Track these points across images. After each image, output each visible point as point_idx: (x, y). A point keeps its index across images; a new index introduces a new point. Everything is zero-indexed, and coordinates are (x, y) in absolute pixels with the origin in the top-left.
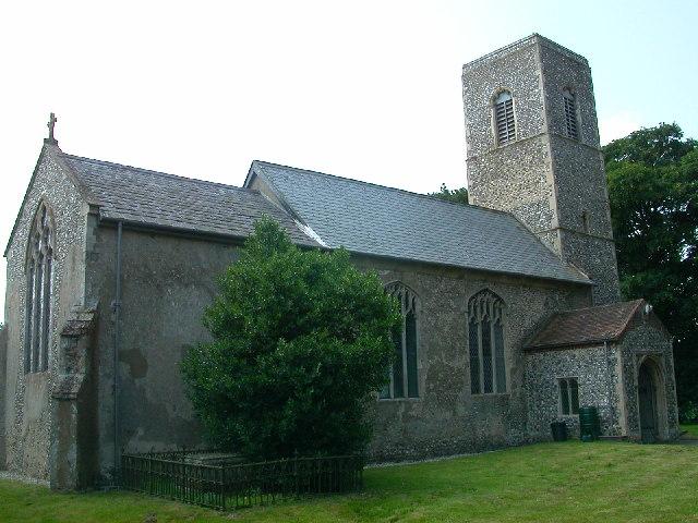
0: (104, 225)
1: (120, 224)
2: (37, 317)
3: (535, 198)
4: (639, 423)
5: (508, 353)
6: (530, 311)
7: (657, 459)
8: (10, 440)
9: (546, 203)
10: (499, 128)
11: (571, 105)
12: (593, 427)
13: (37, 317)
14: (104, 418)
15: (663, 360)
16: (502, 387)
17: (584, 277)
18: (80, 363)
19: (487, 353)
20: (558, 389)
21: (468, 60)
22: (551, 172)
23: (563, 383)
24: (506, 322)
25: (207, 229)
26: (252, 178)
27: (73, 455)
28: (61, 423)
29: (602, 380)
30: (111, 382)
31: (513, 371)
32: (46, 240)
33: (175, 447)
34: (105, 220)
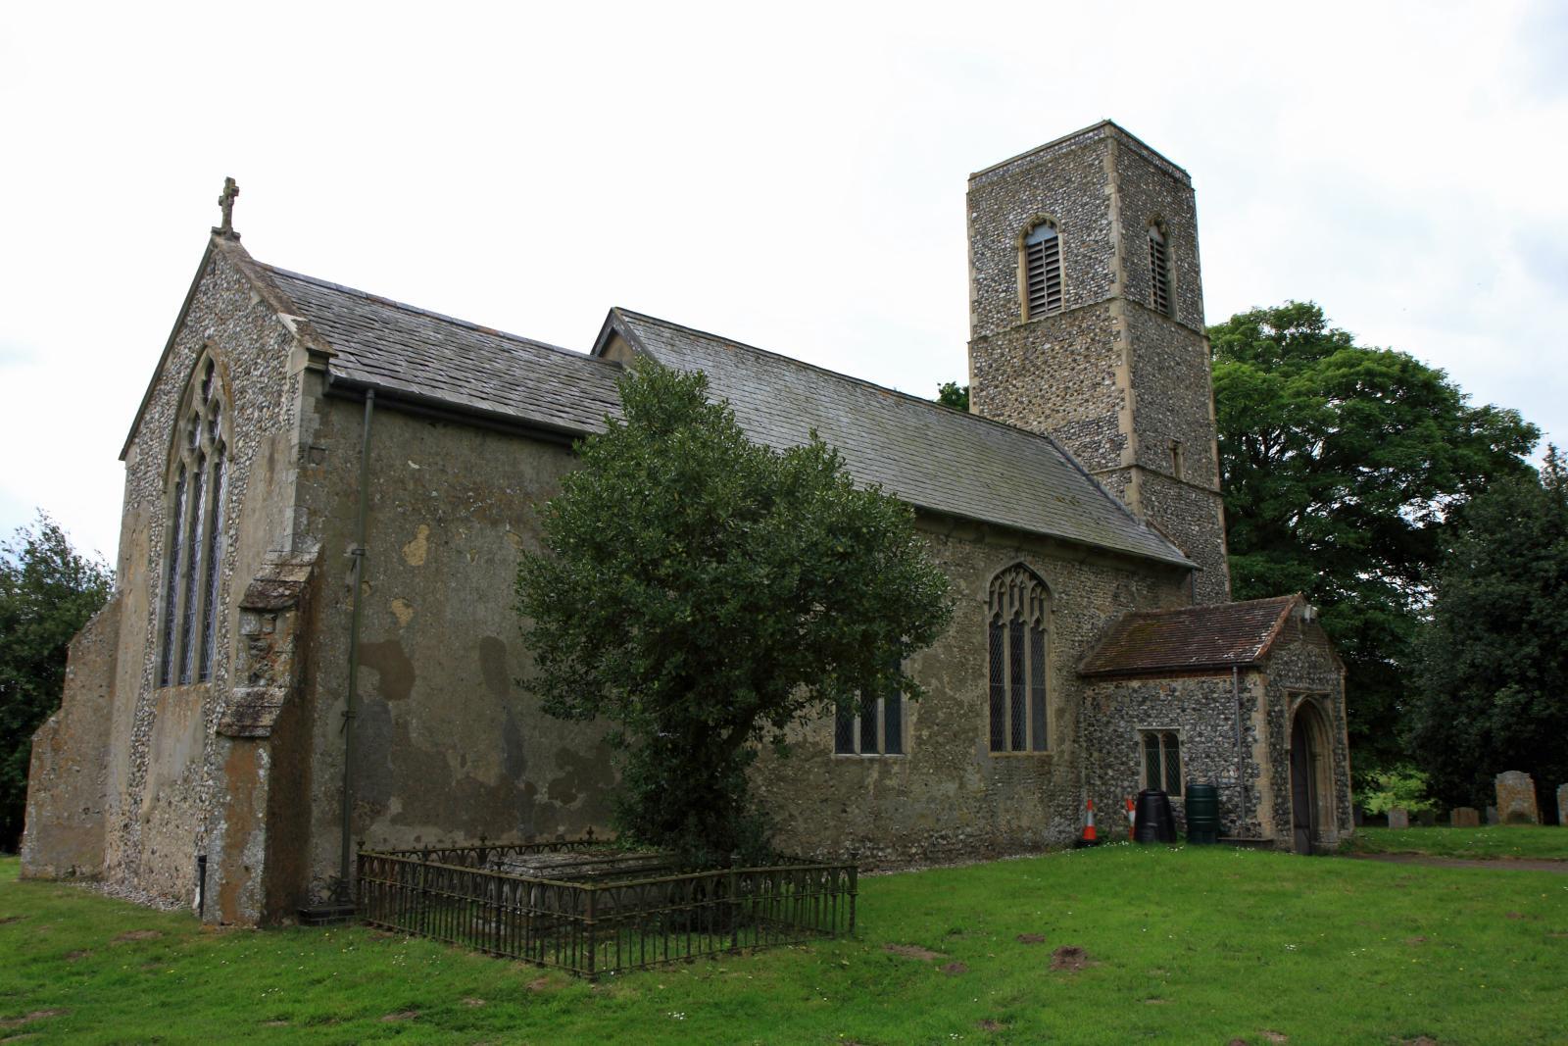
0: (342, 395)
1: (370, 394)
2: (189, 576)
3: (1092, 412)
4: (1291, 816)
5: (1052, 680)
6: (1091, 607)
7: (1327, 889)
8: (115, 820)
9: (1113, 422)
10: (1032, 288)
11: (1160, 252)
12: (1205, 821)
13: (189, 576)
14: (323, 780)
15: (1329, 705)
16: (1040, 742)
17: (1176, 555)
18: (279, 667)
19: (1017, 679)
20: (1142, 749)
21: (979, 167)
22: (1125, 367)
23: (1151, 739)
24: (1050, 625)
25: (538, 417)
26: (609, 336)
27: (256, 854)
28: (233, 789)
29: (1230, 737)
30: (340, 705)
31: (1060, 713)
32: (212, 425)
33: (461, 839)
34: (340, 383)
